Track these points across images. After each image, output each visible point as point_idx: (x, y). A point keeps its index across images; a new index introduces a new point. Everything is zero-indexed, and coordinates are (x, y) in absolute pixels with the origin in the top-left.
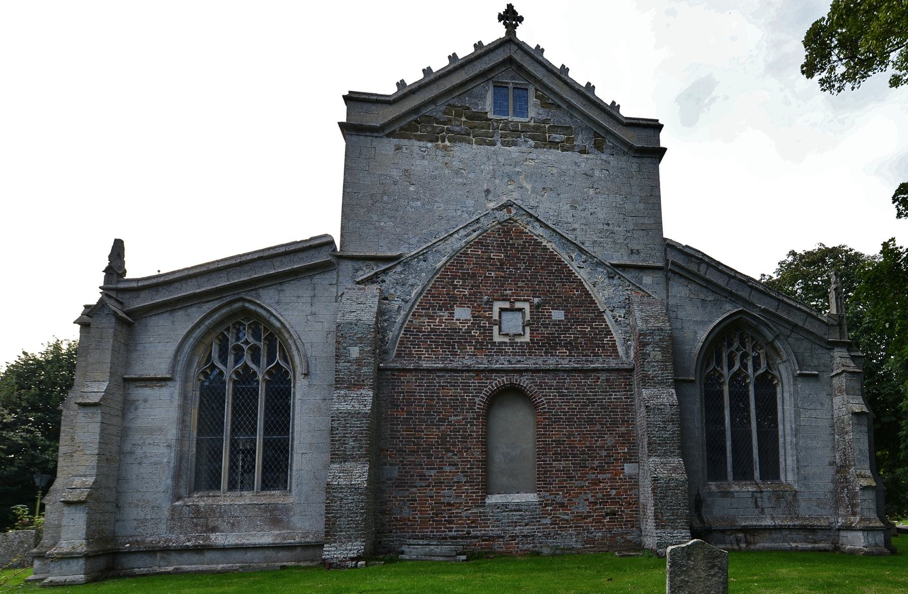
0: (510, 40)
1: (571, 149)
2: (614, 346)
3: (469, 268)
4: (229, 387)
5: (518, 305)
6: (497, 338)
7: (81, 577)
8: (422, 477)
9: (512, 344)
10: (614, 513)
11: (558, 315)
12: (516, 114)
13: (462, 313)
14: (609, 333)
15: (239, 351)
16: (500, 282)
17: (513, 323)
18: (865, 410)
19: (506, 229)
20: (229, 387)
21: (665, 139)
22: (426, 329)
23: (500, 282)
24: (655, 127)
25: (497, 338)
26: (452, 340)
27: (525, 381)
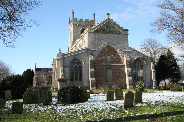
0: (109, 19)
1: (116, 34)
2: (122, 62)
3: (104, 51)
4: (78, 68)
5: (110, 56)
6: (107, 61)
7: (142, 70)
8: (99, 79)
9: (109, 62)
10: (122, 84)
11: (115, 58)
12: (109, 29)
13: (103, 57)
14: (121, 60)
15: (75, 63)
16: (108, 53)
17: (109, 58)
18: (96, 24)
19: (108, 46)
20: (78, 68)
21: (129, 32)
22: (98, 60)
23: (108, 53)
24: (127, 30)
25: (107, 61)
26: (102, 61)
27: (111, 67)
